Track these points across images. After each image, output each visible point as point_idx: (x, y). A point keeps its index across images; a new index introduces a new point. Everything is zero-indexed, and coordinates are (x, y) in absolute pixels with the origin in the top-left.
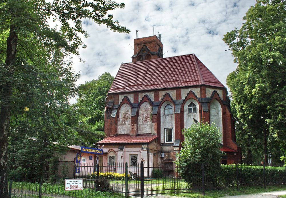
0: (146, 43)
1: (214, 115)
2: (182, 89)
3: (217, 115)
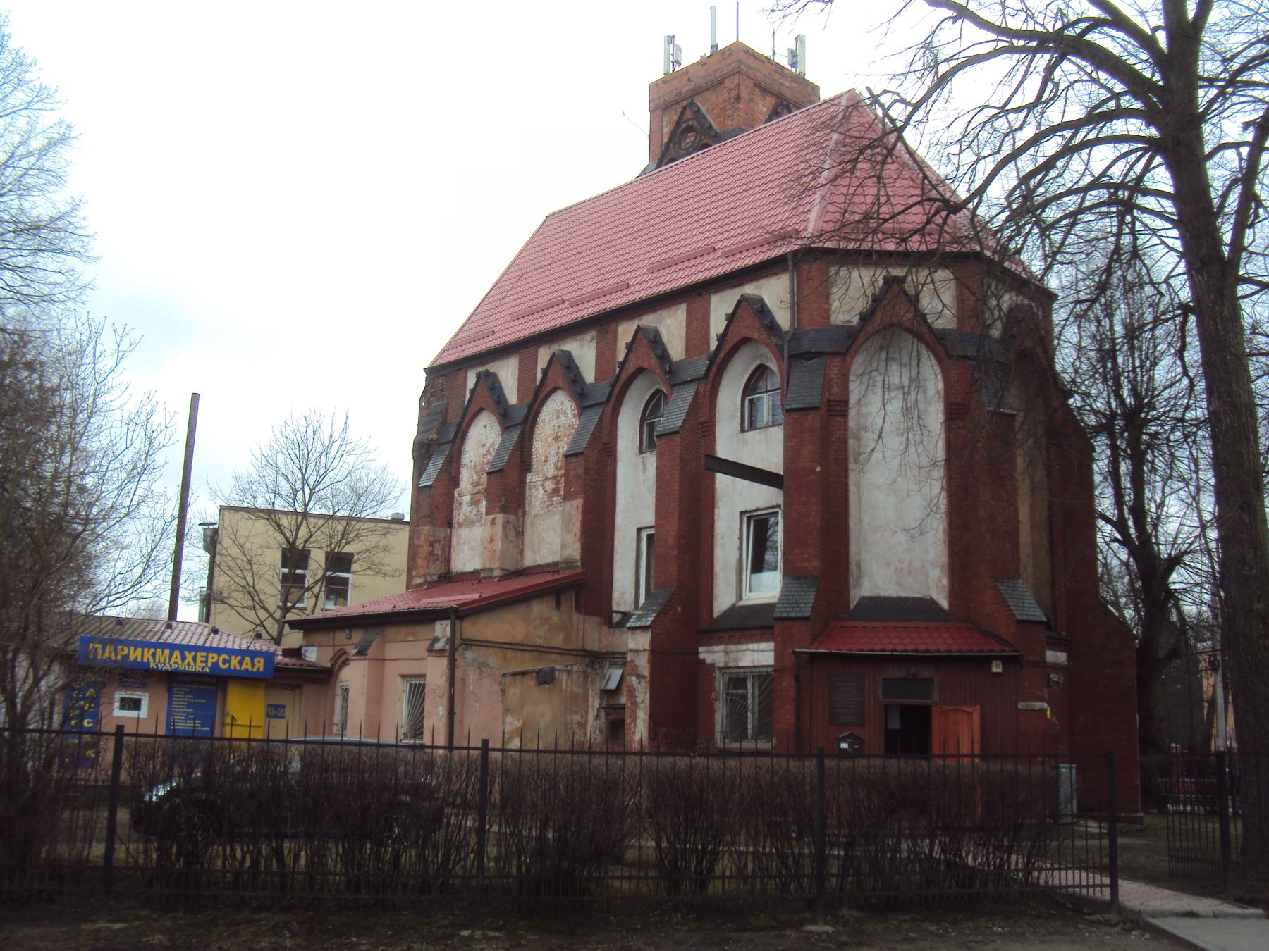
0: (698, 92)
2: (715, 293)
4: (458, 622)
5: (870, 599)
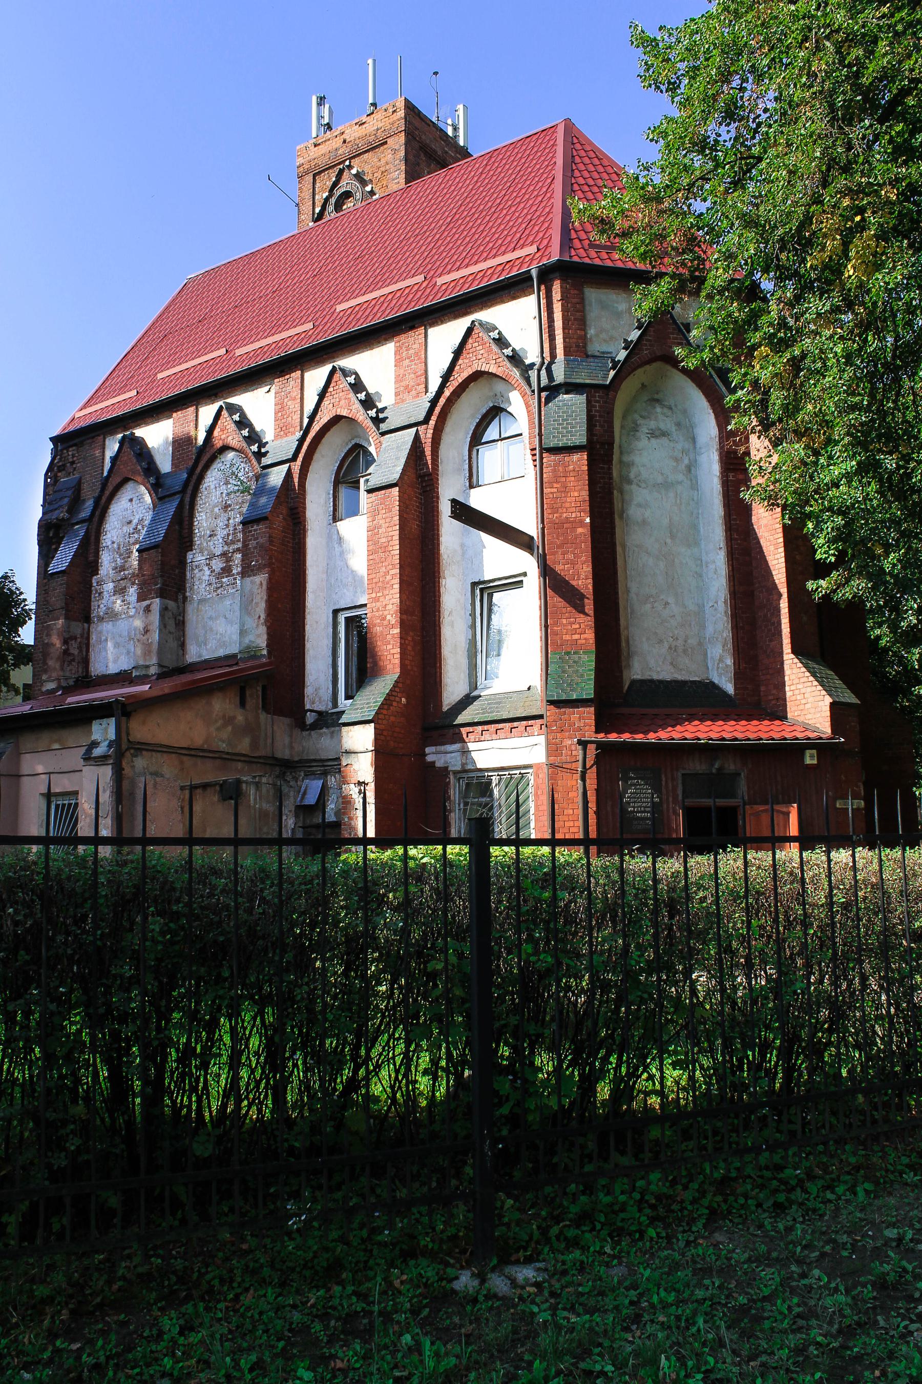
1: (660, 479)
3: (680, 477)
4: (124, 719)
5: (643, 682)
